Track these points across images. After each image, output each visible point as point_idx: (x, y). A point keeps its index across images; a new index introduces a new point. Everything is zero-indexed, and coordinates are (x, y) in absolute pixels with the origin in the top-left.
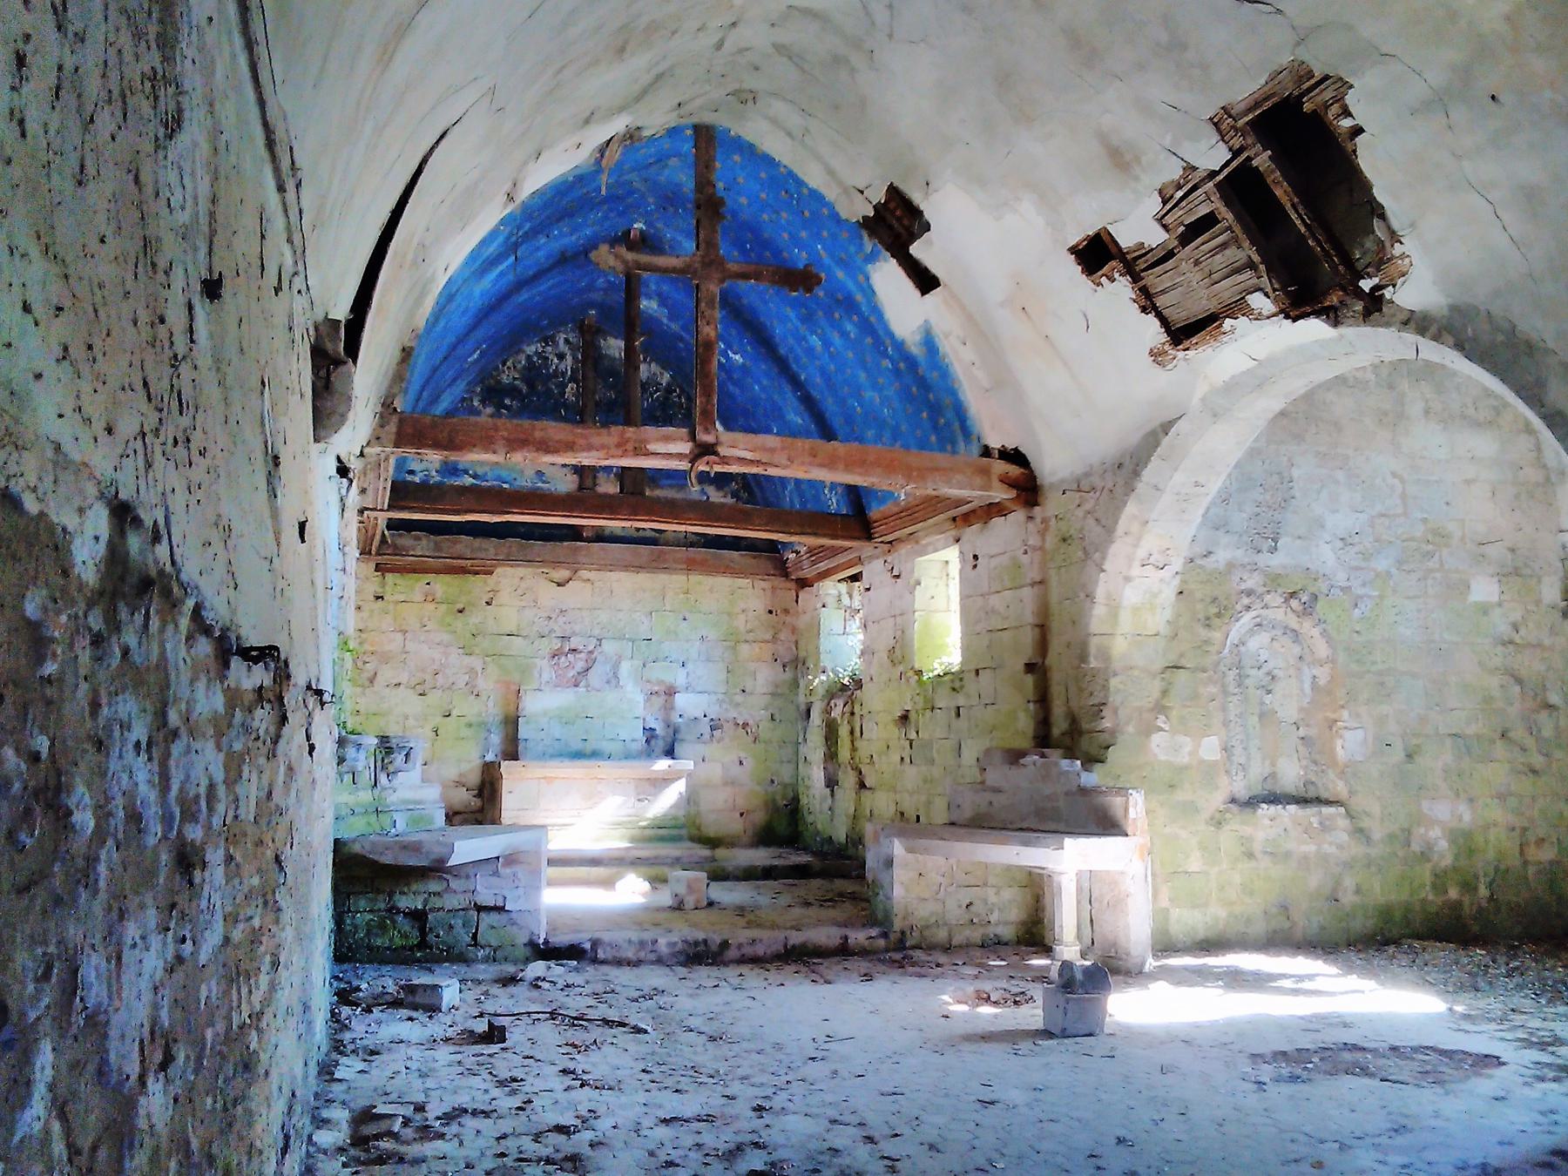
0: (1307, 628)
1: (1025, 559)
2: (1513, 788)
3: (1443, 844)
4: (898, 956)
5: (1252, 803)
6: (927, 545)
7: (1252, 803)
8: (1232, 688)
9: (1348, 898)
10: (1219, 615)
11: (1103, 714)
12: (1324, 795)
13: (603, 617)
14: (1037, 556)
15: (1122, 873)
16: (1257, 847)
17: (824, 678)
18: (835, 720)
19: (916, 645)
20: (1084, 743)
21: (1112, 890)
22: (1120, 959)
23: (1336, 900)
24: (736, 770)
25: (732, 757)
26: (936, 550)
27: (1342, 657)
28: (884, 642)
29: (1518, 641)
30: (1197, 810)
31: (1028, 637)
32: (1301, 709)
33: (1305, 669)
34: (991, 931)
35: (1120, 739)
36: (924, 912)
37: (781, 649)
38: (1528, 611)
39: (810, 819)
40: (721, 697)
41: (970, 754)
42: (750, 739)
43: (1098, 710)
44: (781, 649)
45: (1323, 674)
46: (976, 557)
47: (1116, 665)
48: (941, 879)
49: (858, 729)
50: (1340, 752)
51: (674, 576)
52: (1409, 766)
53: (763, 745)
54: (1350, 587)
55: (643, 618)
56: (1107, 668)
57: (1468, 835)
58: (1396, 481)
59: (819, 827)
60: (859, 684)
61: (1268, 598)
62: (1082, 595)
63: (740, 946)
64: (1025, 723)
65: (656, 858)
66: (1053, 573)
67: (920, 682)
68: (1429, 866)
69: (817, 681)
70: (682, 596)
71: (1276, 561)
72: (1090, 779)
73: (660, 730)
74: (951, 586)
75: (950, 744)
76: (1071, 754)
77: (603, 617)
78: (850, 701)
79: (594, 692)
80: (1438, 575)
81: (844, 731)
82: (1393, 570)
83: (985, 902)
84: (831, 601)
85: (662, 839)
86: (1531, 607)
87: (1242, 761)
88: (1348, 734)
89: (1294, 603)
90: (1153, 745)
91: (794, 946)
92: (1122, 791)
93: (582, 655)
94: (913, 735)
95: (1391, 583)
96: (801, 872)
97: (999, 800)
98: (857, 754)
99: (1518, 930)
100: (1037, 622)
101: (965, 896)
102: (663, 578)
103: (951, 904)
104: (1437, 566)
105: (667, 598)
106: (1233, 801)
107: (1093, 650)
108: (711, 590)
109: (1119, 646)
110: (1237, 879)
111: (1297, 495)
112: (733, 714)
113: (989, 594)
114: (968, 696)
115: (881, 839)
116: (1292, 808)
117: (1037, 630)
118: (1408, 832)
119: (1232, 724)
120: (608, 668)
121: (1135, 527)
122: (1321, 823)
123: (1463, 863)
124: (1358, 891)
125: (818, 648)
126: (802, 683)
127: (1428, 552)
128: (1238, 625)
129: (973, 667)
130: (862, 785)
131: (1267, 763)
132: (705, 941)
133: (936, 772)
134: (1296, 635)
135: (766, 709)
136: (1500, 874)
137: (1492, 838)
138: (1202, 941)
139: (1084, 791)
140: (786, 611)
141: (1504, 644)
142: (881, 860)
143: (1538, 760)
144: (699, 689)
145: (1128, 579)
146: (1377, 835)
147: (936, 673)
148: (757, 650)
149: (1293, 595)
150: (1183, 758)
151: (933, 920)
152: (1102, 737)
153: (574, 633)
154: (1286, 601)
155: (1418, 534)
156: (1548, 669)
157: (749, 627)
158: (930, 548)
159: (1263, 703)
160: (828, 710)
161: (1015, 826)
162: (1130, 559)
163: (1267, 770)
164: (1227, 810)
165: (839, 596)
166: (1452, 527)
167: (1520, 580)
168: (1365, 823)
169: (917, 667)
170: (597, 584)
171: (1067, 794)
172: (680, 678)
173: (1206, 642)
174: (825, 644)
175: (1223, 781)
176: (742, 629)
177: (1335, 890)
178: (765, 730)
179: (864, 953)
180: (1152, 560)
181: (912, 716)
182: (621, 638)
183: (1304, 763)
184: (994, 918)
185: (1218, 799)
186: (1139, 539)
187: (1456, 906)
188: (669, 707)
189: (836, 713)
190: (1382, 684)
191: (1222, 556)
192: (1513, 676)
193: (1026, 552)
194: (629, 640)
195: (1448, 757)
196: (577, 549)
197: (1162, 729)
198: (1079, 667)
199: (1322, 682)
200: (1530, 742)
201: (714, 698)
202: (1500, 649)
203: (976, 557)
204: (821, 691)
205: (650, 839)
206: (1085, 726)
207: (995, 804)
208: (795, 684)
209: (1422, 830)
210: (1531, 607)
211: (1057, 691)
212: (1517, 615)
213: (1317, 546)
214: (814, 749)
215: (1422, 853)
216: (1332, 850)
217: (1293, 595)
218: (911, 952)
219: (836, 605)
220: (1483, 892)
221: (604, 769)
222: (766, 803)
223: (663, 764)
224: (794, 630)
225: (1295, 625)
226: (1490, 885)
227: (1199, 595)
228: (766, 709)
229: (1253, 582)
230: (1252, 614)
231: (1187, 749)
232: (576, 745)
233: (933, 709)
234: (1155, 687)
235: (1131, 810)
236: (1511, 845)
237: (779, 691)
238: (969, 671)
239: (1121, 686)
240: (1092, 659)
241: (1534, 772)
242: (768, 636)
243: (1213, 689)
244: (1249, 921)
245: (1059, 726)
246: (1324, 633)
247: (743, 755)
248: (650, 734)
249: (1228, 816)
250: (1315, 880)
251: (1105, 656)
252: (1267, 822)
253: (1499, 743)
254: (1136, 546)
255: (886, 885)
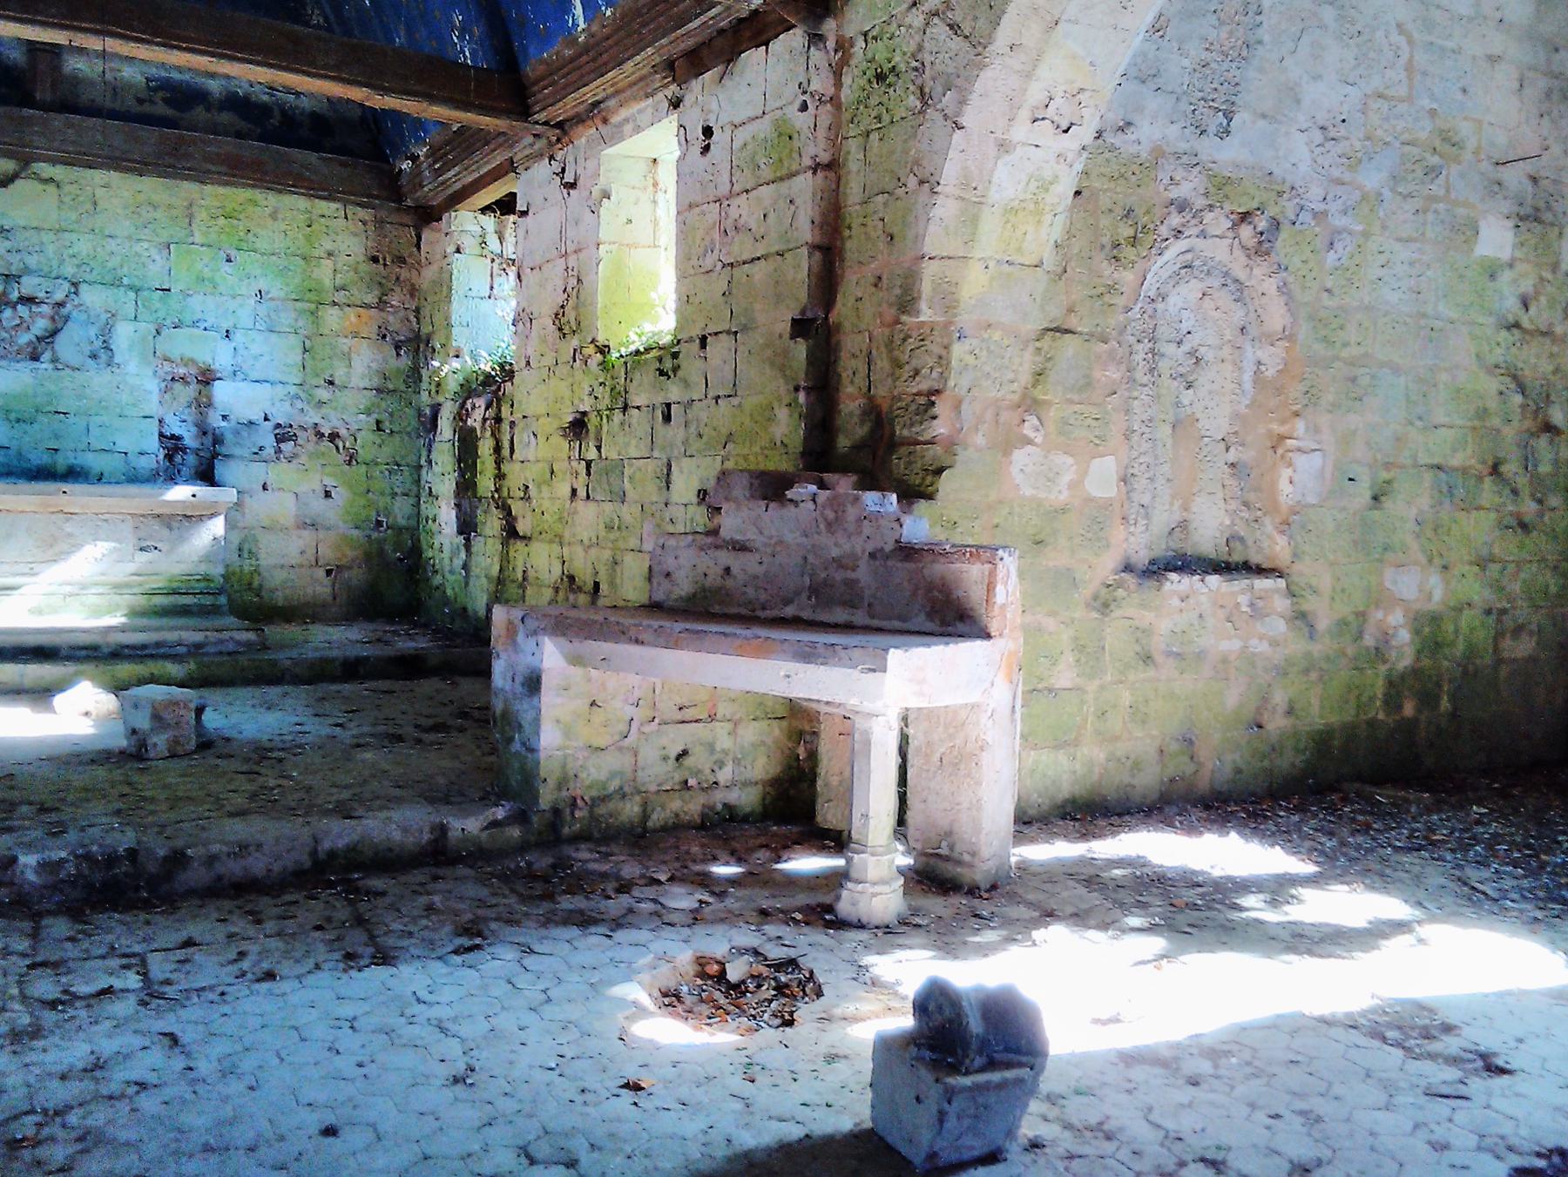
0: (1261, 279)
1: (802, 121)
2: (1496, 551)
3: (1405, 636)
4: (543, 862)
5: (1157, 569)
6: (620, 125)
7: (1157, 569)
8: (1140, 376)
9: (1277, 724)
10: (1134, 241)
11: (936, 410)
12: (1255, 559)
13: (83, 246)
14: (825, 115)
15: (974, 707)
16: (1157, 645)
17: (456, 364)
18: (473, 430)
19: (601, 300)
20: (898, 464)
21: (951, 737)
22: (959, 863)
23: (1260, 727)
24: (318, 505)
25: (313, 483)
26: (638, 129)
27: (1304, 330)
28: (545, 309)
29: (1526, 323)
30: (1075, 583)
31: (800, 269)
32: (1236, 416)
33: (1248, 347)
34: (719, 798)
35: (963, 456)
36: (597, 772)
37: (394, 322)
38: (1542, 279)
39: (437, 580)
40: (293, 390)
41: (685, 485)
42: (343, 457)
43: (927, 404)
44: (394, 322)
45: (1272, 358)
46: (708, 132)
47: (966, 318)
48: (630, 711)
49: (506, 444)
50: (1284, 487)
51: (208, 188)
52: (1376, 514)
53: (363, 469)
54: (1325, 213)
55: (154, 253)
56: (949, 323)
57: (1435, 619)
58: (1401, 41)
59: (449, 592)
60: (508, 372)
61: (1208, 217)
62: (912, 182)
63: (212, 859)
64: (787, 427)
65: (158, 645)
66: (853, 146)
67: (603, 365)
68: (1383, 668)
69: (446, 368)
70: (222, 221)
71: (1227, 154)
72: (919, 526)
73: (190, 438)
74: (661, 203)
75: (652, 467)
76: (870, 481)
77: (83, 245)
78: (496, 400)
79: (68, 371)
80: (1441, 207)
81: (485, 447)
82: (1387, 193)
83: (711, 747)
84: (470, 244)
85: (184, 611)
86: (1548, 275)
87: (1146, 500)
88: (1300, 460)
89: (1246, 231)
90: (1014, 470)
91: (332, 854)
92: (985, 553)
93: (45, 309)
94: (592, 454)
95: (1381, 214)
96: (409, 667)
97: (743, 565)
98: (506, 483)
99: (215, 421)
100: (818, 240)
101: (675, 740)
102: (189, 188)
103: (649, 754)
104: (1442, 192)
105: (196, 221)
106: (1128, 568)
107: (926, 288)
108: (274, 216)
109: (974, 283)
110: (1126, 698)
111: (1266, 38)
112: (312, 417)
113: (731, 195)
114: (686, 384)
115: (520, 637)
116: (1214, 580)
117: (818, 255)
118: (1362, 615)
119: (1135, 437)
120: (93, 331)
121: (1032, 35)
122: (1252, 605)
123: (1426, 662)
124: (1290, 712)
125: (447, 318)
126: (424, 372)
127: (1433, 169)
128: (1161, 261)
129: (697, 332)
130: (511, 532)
131: (1177, 504)
132: (132, 854)
133: (629, 512)
134: (1240, 291)
135: (368, 412)
136: (1468, 671)
137: (1463, 624)
138: (1063, 805)
139: (907, 552)
140: (400, 260)
141: (1508, 328)
142: (519, 680)
143: (1529, 507)
144: (255, 376)
145: (1004, 147)
146: (1323, 624)
147: (632, 348)
148: (353, 319)
149: (1245, 217)
150: (1060, 495)
151: (614, 785)
152: (938, 450)
153: (27, 270)
154: (1235, 226)
155: (1423, 135)
156: (1556, 371)
157: (338, 282)
158: (628, 128)
159: (1178, 404)
160: (461, 416)
161: (768, 613)
162: (1013, 104)
163: (1177, 516)
164: (1120, 584)
165: (483, 236)
166: (1465, 129)
167: (1538, 228)
168: (1310, 604)
169: (601, 340)
170: (67, 188)
171: (872, 556)
172: (220, 356)
173: (1111, 288)
174: (459, 310)
175: (1118, 533)
176: (328, 283)
177: (1259, 710)
178: (366, 444)
179: (476, 856)
180: (1050, 112)
181: (593, 421)
182: (116, 283)
183: (1234, 505)
184: (724, 776)
185: (1107, 564)
186: (1037, 61)
187: (1409, 726)
188: (203, 404)
189: (475, 421)
190: (1354, 380)
191: (1148, 133)
192: (1514, 377)
193: (804, 107)
194: (131, 287)
195: (1424, 502)
196: (29, 121)
197: (1030, 442)
198: (897, 322)
199: (1270, 373)
200: (1522, 481)
201: (280, 391)
202: (1504, 333)
203: (708, 132)
204: (452, 385)
205: (143, 613)
206: (901, 432)
207: (735, 570)
208: (414, 375)
209: (1380, 615)
210: (1548, 275)
211: (850, 367)
212: (1527, 286)
213: (1287, 133)
214: (442, 478)
215: (1377, 649)
216: (1262, 647)
217: (1245, 217)
218: (569, 850)
219: (478, 250)
220: (1445, 704)
221: (76, 496)
222: (368, 557)
223: (181, 493)
224: (413, 291)
225: (1241, 274)
226: (1453, 698)
227: (1105, 201)
228: (368, 412)
229: (1190, 187)
230: (1182, 245)
231: (1067, 478)
232: (38, 458)
233: (625, 408)
234: (1025, 364)
235: (1000, 589)
236: (1483, 636)
237: (391, 387)
238: (691, 340)
239: (970, 360)
240: (923, 306)
241: (1524, 526)
242: (371, 298)
243: (1114, 374)
244: (1137, 766)
245: (851, 431)
246: (1283, 289)
247: (329, 482)
248: (172, 445)
249: (1120, 593)
250: (1233, 697)
251: (949, 302)
252: (1176, 602)
253: (1488, 480)
254: (1028, 76)
255: (526, 718)
